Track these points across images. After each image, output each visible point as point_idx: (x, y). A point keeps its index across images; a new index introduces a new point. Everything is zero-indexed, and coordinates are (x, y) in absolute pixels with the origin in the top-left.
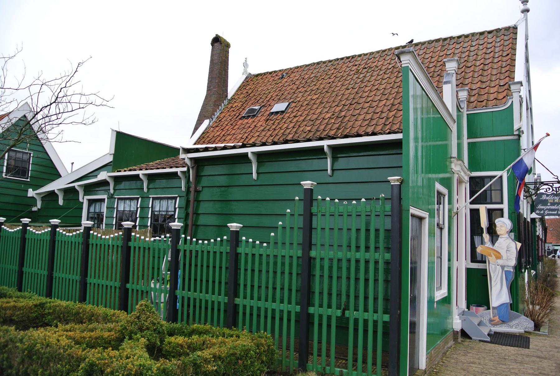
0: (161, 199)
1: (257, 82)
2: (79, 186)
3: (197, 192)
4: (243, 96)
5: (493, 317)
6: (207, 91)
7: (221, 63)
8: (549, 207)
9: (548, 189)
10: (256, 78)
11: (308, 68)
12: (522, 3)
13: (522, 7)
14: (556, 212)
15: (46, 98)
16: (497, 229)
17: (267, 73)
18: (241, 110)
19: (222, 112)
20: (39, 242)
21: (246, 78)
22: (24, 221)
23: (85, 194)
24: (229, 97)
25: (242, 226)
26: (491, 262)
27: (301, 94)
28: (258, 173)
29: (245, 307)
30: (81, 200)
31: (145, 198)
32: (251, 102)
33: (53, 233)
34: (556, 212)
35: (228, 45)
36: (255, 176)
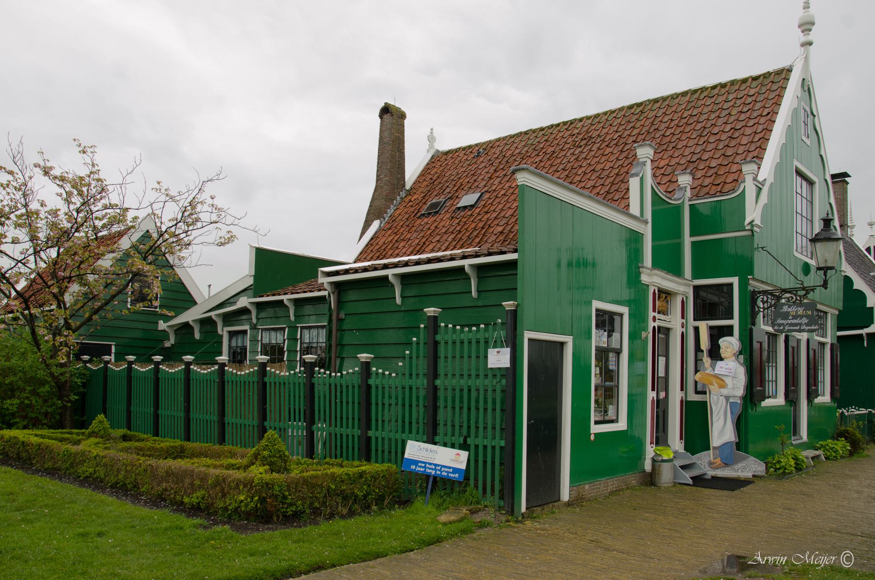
0: (310, 328)
1: (446, 163)
2: (217, 315)
3: (340, 320)
4: (425, 183)
5: (714, 459)
6: (377, 181)
7: (393, 141)
8: (790, 322)
9: (790, 299)
10: (444, 157)
11: (512, 140)
12: (803, 32)
13: (803, 39)
14: (798, 328)
15: (170, 213)
16: (721, 351)
17: (459, 149)
18: (421, 205)
19: (397, 209)
20: (173, 381)
21: (432, 157)
22: (156, 358)
23: (224, 326)
24: (408, 187)
25: (373, 356)
26: (712, 392)
27: (499, 180)
28: (402, 297)
29: (377, 438)
30: (220, 332)
31: (293, 329)
32: (435, 193)
33: (187, 370)
34: (798, 328)
35: (403, 116)
36: (398, 300)
